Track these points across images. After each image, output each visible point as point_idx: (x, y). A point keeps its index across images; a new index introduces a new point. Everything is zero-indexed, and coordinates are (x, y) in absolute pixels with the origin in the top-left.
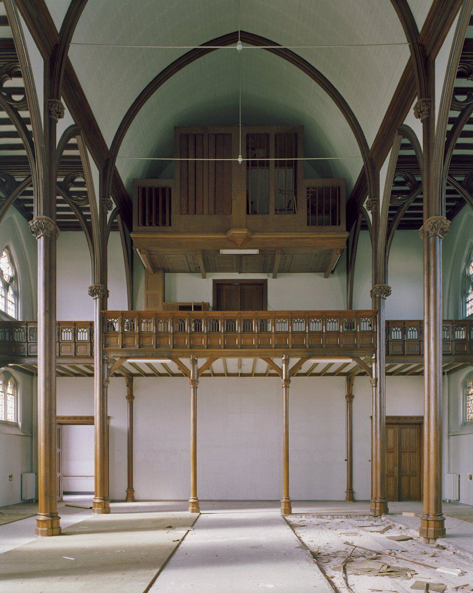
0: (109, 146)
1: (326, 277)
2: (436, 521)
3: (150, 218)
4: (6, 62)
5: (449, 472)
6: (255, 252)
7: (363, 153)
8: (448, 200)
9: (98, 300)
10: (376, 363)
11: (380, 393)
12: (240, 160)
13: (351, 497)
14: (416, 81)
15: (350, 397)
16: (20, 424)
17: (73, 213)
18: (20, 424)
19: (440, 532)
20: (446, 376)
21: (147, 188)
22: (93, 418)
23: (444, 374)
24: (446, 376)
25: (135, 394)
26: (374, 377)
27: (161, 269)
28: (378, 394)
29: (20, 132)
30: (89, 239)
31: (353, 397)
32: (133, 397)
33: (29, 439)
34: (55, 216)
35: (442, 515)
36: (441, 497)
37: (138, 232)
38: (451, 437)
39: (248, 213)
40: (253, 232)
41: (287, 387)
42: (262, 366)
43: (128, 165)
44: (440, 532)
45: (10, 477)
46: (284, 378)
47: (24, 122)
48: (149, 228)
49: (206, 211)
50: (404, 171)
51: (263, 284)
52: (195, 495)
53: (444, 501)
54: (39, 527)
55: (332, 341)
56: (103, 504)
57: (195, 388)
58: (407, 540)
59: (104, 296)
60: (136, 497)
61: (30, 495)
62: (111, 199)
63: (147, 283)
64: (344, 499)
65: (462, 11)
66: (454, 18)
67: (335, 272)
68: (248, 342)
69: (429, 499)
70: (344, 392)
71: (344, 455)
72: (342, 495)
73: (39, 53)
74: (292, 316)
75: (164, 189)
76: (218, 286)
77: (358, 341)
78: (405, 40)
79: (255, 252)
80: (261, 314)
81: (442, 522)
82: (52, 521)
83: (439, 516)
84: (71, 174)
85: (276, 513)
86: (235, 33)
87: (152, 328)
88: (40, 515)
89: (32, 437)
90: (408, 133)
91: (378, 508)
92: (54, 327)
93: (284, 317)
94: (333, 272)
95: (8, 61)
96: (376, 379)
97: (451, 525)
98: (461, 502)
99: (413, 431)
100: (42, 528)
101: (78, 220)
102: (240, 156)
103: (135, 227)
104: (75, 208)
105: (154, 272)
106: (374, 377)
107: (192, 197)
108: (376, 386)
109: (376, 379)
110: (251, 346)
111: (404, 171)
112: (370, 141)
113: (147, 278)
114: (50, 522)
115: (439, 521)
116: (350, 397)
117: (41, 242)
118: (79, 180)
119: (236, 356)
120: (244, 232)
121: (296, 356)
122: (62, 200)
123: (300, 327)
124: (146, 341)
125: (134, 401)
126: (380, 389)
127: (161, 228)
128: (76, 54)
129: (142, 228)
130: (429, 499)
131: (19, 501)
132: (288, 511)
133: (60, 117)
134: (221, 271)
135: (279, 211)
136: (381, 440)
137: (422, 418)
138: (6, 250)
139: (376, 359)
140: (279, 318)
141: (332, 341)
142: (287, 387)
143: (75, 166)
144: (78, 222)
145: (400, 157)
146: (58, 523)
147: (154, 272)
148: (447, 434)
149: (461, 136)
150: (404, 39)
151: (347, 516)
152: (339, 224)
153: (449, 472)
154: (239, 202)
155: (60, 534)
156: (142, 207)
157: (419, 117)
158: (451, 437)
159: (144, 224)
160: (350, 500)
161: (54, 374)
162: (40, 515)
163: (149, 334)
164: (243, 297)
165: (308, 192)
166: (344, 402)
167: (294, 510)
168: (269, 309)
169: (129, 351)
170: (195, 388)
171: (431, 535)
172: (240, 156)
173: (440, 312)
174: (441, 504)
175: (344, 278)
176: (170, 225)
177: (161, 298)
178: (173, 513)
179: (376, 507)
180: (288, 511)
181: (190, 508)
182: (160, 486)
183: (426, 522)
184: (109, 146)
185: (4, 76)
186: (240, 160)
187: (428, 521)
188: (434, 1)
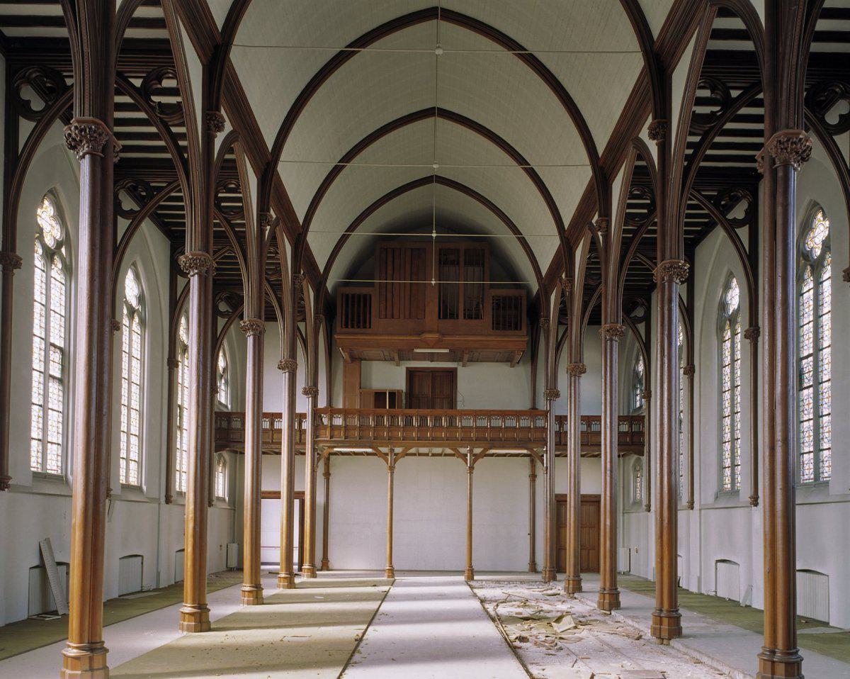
0: (322, 271)
1: (512, 366)
2: (670, 617)
3: (353, 320)
4: (155, 66)
5: (624, 546)
6: (447, 351)
7: (560, 233)
8: (686, 232)
9: (287, 374)
10: (547, 454)
11: (550, 479)
12: (433, 282)
13: (533, 568)
14: (564, 256)
15: (533, 477)
16: (227, 499)
17: (162, 143)
18: (227, 499)
19: (676, 632)
20: (621, 458)
21: (350, 296)
22: (279, 493)
23: (619, 456)
24: (621, 458)
25: (331, 472)
26: (545, 466)
27: (356, 359)
28: (548, 480)
29: (139, 103)
30: (304, 348)
31: (536, 476)
32: (329, 474)
33: (233, 511)
34: (111, 123)
35: (677, 611)
36: (616, 570)
37: (340, 334)
38: (625, 515)
39: (439, 318)
40: (443, 335)
41: (471, 473)
42: (448, 451)
43: (330, 285)
44: (676, 632)
45: (221, 546)
46: (469, 465)
47: (175, 138)
48: (351, 330)
49: (402, 316)
50: (643, 185)
51: (452, 374)
52: (391, 563)
53: (620, 573)
54: (67, 668)
55: (509, 435)
56: (255, 593)
57: (392, 473)
58: (555, 595)
59: (260, 333)
60: (330, 567)
61: (234, 563)
62: (223, 112)
63: (345, 371)
64: (527, 570)
65: (699, 32)
66: (621, 166)
67: (521, 362)
68: (438, 434)
69: (605, 570)
70: (528, 472)
71: (527, 530)
72: (526, 567)
73: (199, 60)
74: (476, 414)
75: (365, 296)
76: (411, 374)
77: (527, 436)
78: (638, 48)
79: (447, 351)
80: (451, 412)
81: (678, 618)
82: (91, 659)
83: (673, 611)
84: (155, 69)
85: (462, 578)
86: (433, 8)
87: (357, 423)
88: (69, 646)
89: (235, 510)
90: (643, 153)
91: (571, 586)
92: (259, 414)
93: (469, 415)
94: (518, 363)
95: (158, 66)
96: (547, 467)
97: (625, 599)
98: (631, 573)
99: (592, 508)
100: (72, 670)
101: (223, 229)
102: (434, 231)
103: (338, 329)
104: (225, 223)
105: (352, 362)
106: (545, 466)
107: (389, 303)
108: (547, 473)
109: (547, 467)
110: (442, 439)
111: (643, 185)
112: (567, 222)
113: (345, 367)
114: (198, 615)
115: (674, 617)
116: (533, 477)
117: (250, 341)
118: (168, 83)
119: (427, 446)
120: (436, 336)
121: (479, 447)
122: (154, 133)
123: (484, 423)
124: (351, 433)
125: (330, 478)
126: (550, 476)
127: (362, 330)
128: (283, 169)
129: (345, 330)
130: (605, 570)
131: (224, 568)
132: (471, 578)
133: (219, 131)
134: (414, 360)
135: (469, 316)
136: (550, 518)
137: (600, 496)
138: (133, 267)
139: (547, 450)
140: (465, 415)
141: (509, 435)
142: (471, 473)
143: (230, 170)
144: (219, 223)
145: (637, 167)
146: (208, 616)
147: (352, 362)
148: (621, 511)
149: (704, 161)
150: (587, 161)
151: (521, 582)
152: (521, 329)
153: (624, 546)
154: (432, 308)
155: (210, 630)
156: (343, 314)
157: (654, 139)
158: (625, 515)
159: (347, 326)
160: (532, 571)
161: (260, 453)
162: (69, 646)
163: (354, 428)
164: (432, 392)
165: (493, 300)
166: (527, 481)
167: (476, 578)
168: (458, 408)
169: (335, 442)
170: (392, 473)
171: (571, 591)
172: (434, 231)
173: (615, 407)
174: (615, 574)
175: (529, 369)
176: (370, 327)
177: (358, 386)
178: (323, 629)
179: (604, 600)
180: (471, 578)
181: (386, 574)
182: (353, 558)
183: (659, 618)
184: (322, 271)
185: (154, 82)
186: (433, 282)
187: (661, 617)
188: (675, 2)
